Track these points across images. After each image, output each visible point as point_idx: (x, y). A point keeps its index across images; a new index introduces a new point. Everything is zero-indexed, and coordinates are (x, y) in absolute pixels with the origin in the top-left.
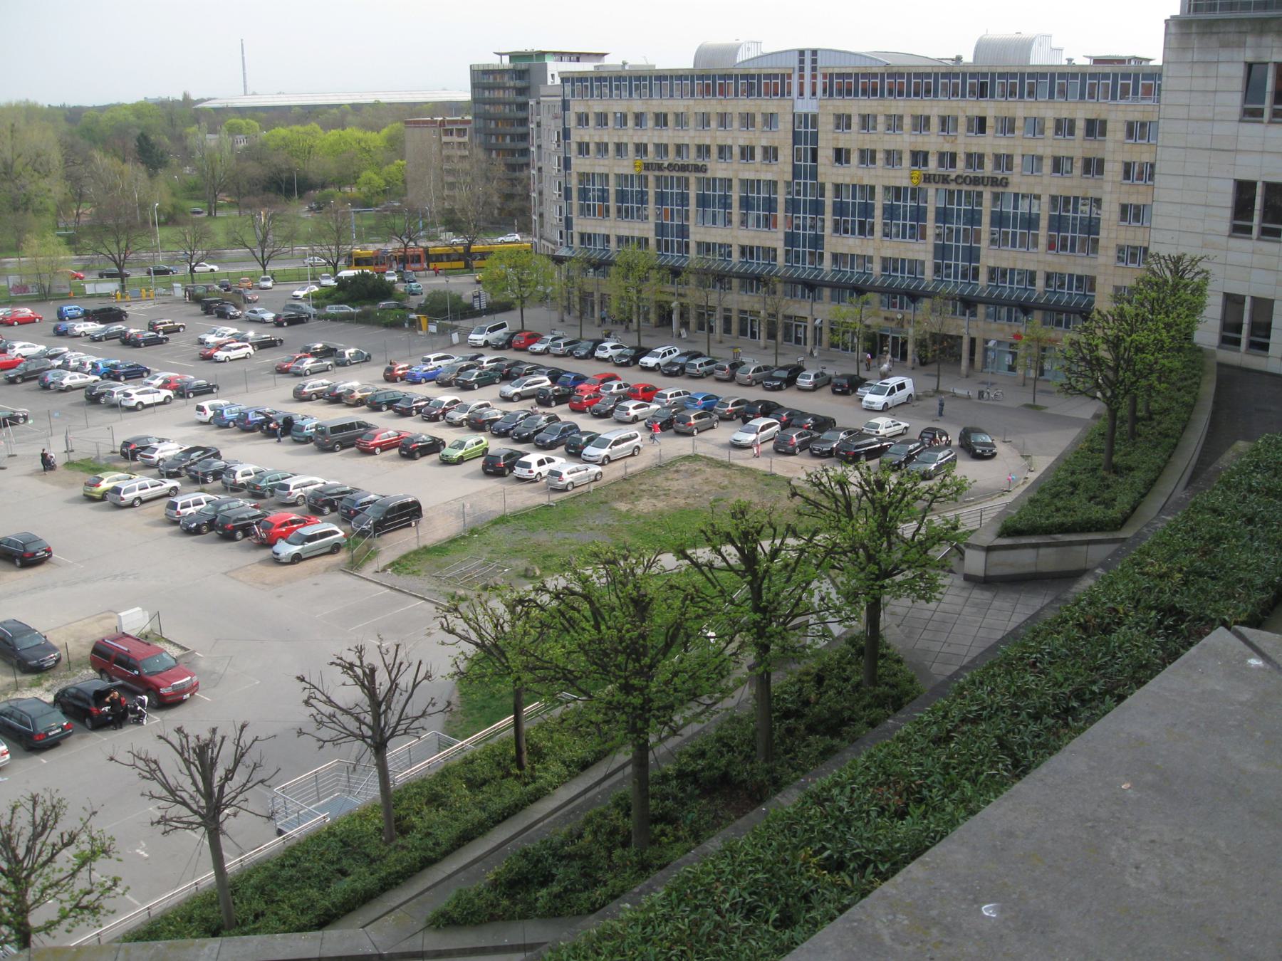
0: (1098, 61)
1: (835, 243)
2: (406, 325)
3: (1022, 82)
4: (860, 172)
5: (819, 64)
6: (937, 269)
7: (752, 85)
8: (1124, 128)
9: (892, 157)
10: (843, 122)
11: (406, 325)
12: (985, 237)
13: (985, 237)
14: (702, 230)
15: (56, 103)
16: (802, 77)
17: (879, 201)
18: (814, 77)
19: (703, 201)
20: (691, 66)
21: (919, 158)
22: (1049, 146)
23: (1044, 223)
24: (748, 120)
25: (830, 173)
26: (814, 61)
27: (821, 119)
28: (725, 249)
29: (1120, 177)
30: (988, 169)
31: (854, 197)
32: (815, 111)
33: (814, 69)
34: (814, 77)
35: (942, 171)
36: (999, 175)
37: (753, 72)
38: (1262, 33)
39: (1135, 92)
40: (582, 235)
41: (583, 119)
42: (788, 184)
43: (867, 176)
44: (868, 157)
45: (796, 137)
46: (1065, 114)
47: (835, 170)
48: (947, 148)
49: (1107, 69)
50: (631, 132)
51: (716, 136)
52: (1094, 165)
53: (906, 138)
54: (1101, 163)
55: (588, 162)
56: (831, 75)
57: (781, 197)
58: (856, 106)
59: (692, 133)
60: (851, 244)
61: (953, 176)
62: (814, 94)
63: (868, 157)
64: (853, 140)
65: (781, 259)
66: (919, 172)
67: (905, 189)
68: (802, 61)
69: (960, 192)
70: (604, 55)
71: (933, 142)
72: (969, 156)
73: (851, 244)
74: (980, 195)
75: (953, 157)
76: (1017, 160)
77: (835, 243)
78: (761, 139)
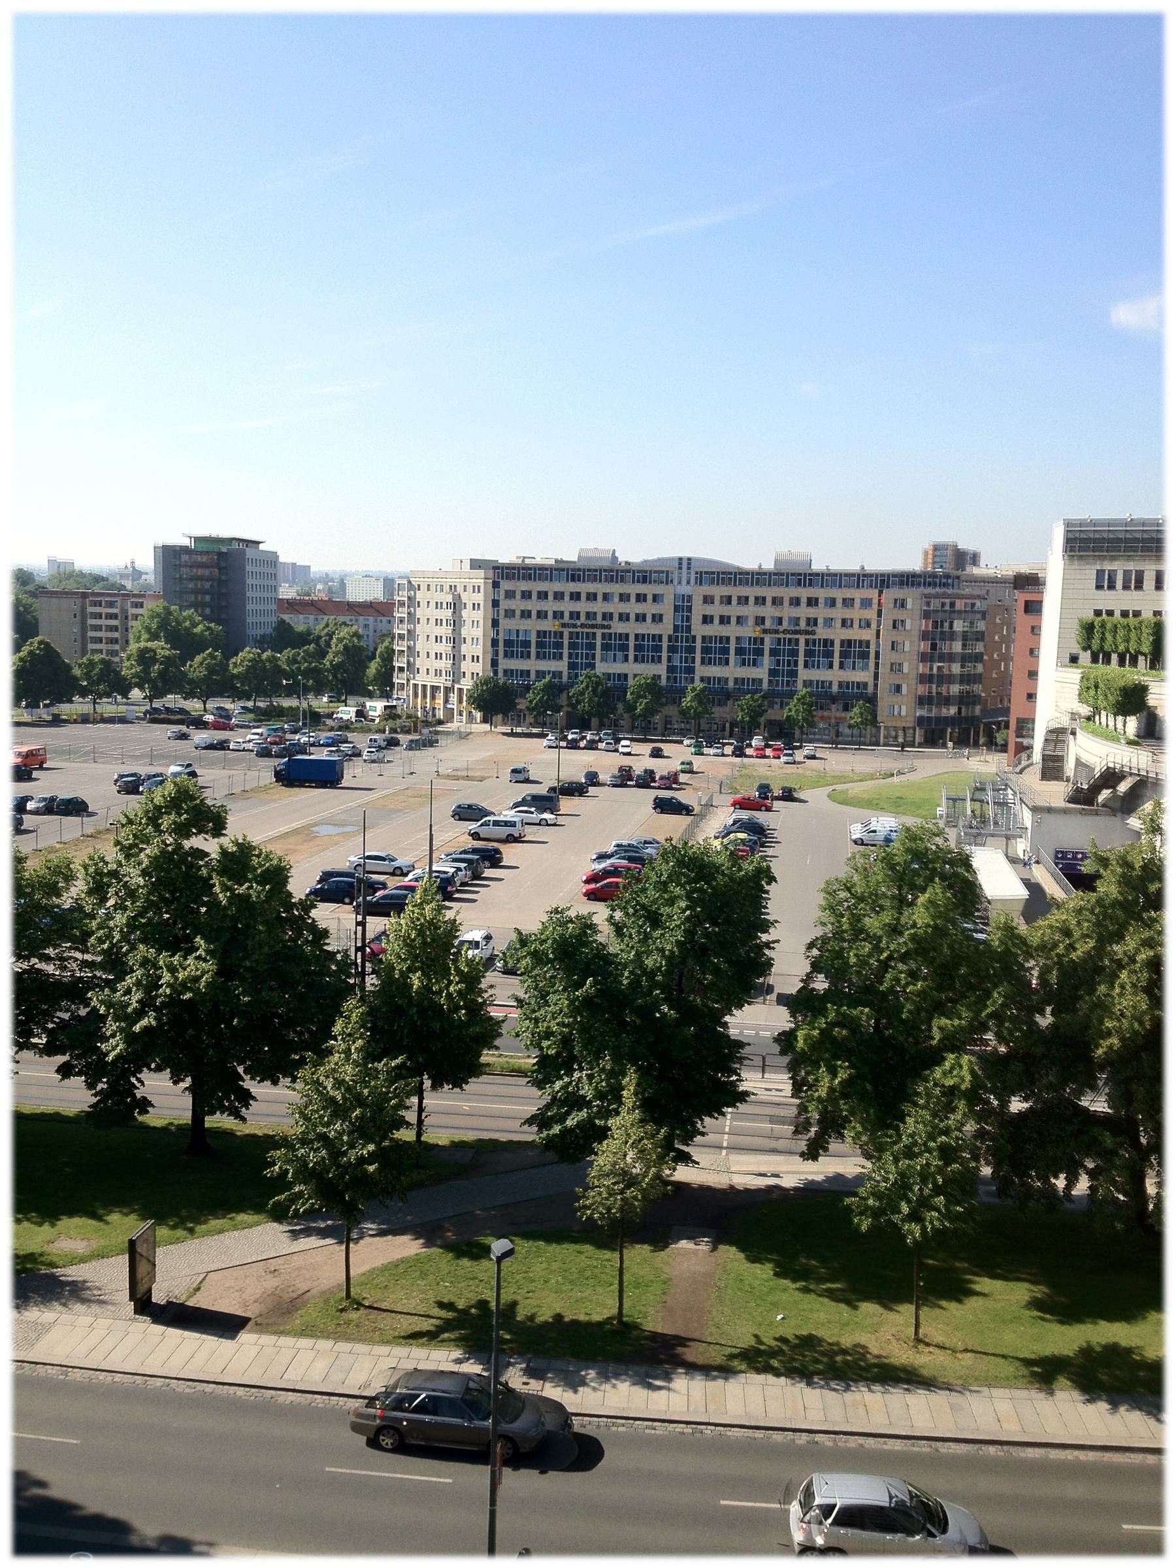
10: (708, 600)
23: (533, 645)
25: (699, 630)
26: (689, 564)
33: (689, 568)
40: (505, 671)
42: (670, 638)
43: (724, 631)
44: (724, 620)
48: (778, 614)
51: (615, 607)
56: (701, 572)
57: (665, 644)
58: (718, 591)
59: (551, 603)
62: (688, 583)
63: (724, 620)
64: (716, 610)
69: (582, 633)
78: (649, 608)
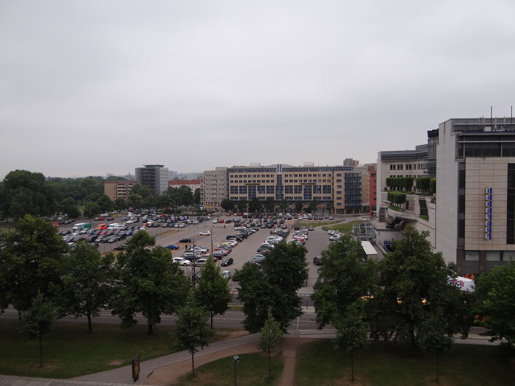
0: (147, 166)
2: (202, 215)
4: (290, 183)
7: (311, 170)
8: (336, 175)
9: (241, 181)
11: (202, 215)
16: (278, 169)
18: (281, 169)
20: (303, 166)
21: (245, 181)
22: (322, 178)
24: (245, 176)
25: (284, 184)
26: (281, 166)
27: (282, 176)
28: (291, 198)
29: (336, 182)
30: (257, 182)
33: (281, 167)
34: (281, 169)
35: (304, 183)
36: (258, 183)
38: (391, 162)
39: (340, 170)
41: (232, 176)
42: (276, 186)
45: (278, 178)
48: (305, 179)
49: (149, 168)
51: (261, 179)
52: (291, 181)
54: (273, 181)
58: (289, 173)
59: (247, 178)
60: (289, 195)
61: (307, 183)
62: (281, 171)
64: (288, 178)
65: (275, 198)
67: (298, 186)
68: (278, 166)
74: (255, 186)
76: (317, 180)
77: (285, 195)
78: (270, 179)
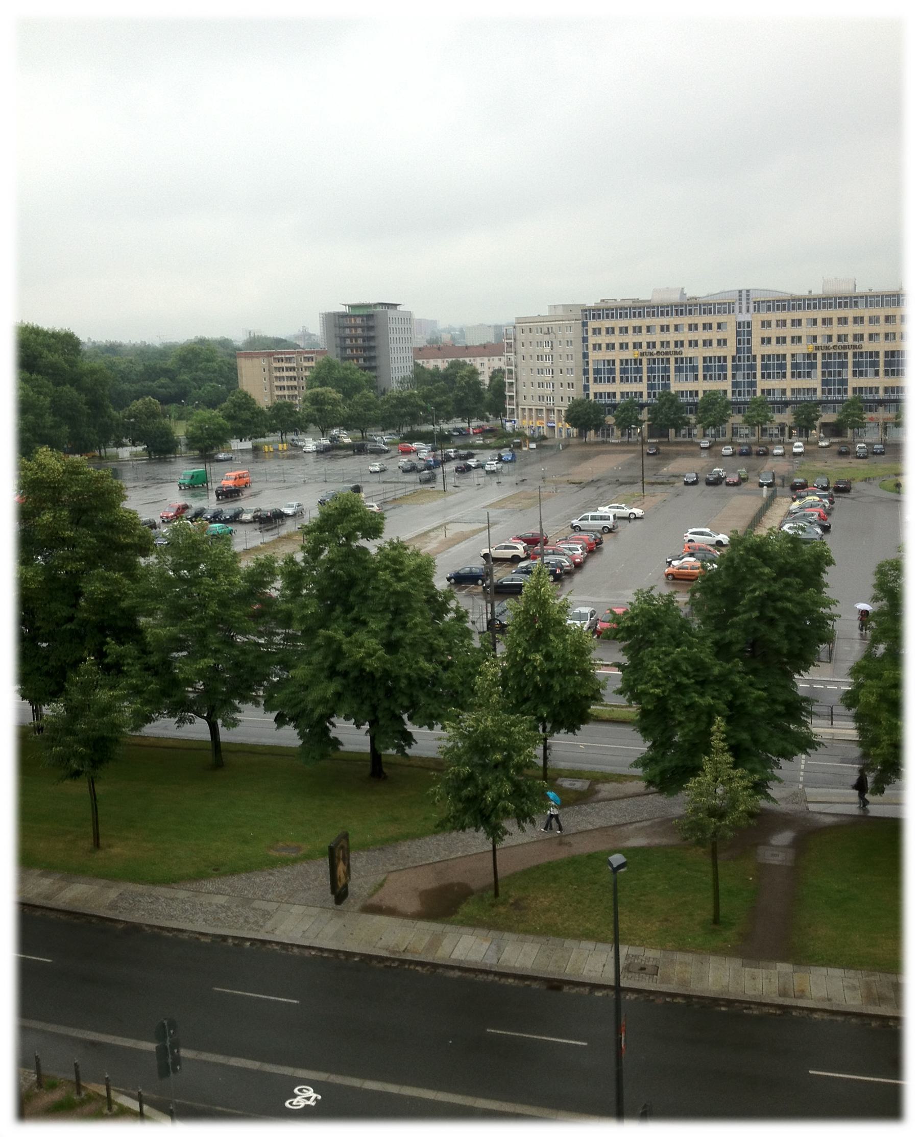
1: (762, 384)
3: (715, 307)
5: (751, 297)
6: (733, 392)
9: (797, 339)
10: (765, 324)
12: (759, 375)
13: (759, 375)
14: (679, 384)
15: (272, 336)
16: (740, 303)
17: (618, 367)
18: (748, 303)
19: (678, 370)
25: (758, 350)
26: (748, 295)
31: (604, 366)
32: (750, 319)
33: (748, 299)
35: (649, 350)
37: (711, 302)
41: (597, 331)
43: (610, 355)
46: (859, 315)
47: (762, 348)
50: (631, 336)
53: (658, 335)
55: (601, 354)
58: (773, 316)
59: (672, 335)
60: (773, 384)
61: (831, 346)
62: (748, 311)
66: (637, 352)
68: (740, 296)
69: (658, 359)
70: (396, 305)
71: (644, 338)
72: (648, 343)
73: (773, 384)
74: (668, 359)
75: (654, 343)
77: (762, 384)
78: (714, 335)
